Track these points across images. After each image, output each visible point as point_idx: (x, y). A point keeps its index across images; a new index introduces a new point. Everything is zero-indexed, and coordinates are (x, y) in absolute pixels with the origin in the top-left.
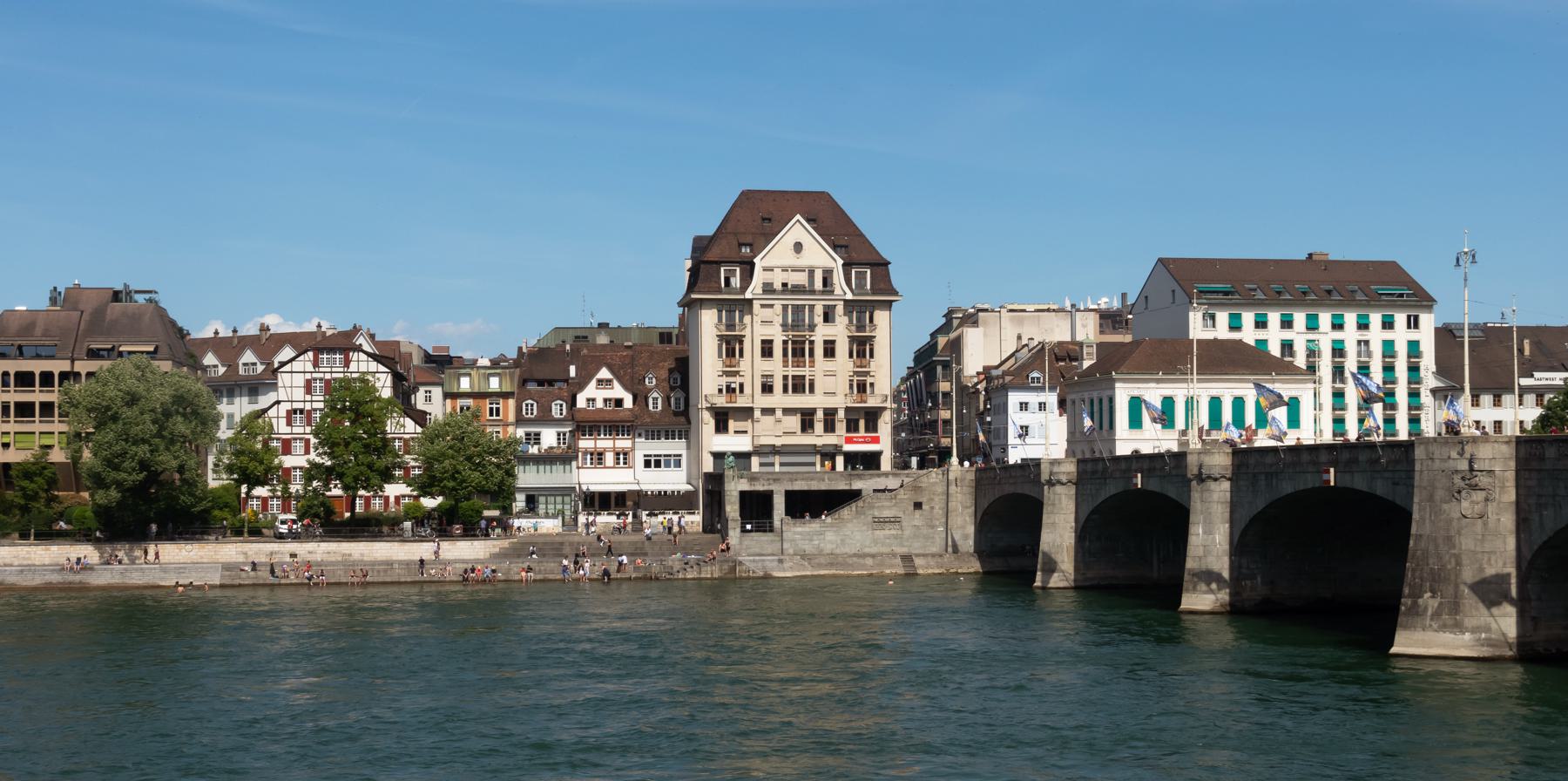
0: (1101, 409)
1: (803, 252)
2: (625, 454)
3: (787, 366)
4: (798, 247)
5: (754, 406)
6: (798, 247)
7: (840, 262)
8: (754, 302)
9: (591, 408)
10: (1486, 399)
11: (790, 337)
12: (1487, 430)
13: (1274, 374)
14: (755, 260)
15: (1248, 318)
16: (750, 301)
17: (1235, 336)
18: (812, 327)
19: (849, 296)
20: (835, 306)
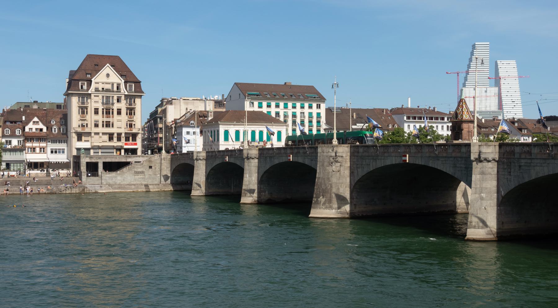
1: (110, 77)
2: (44, 148)
4: (108, 75)
7: (123, 81)
8: (92, 94)
14: (92, 80)
15: (265, 104)
18: (113, 104)
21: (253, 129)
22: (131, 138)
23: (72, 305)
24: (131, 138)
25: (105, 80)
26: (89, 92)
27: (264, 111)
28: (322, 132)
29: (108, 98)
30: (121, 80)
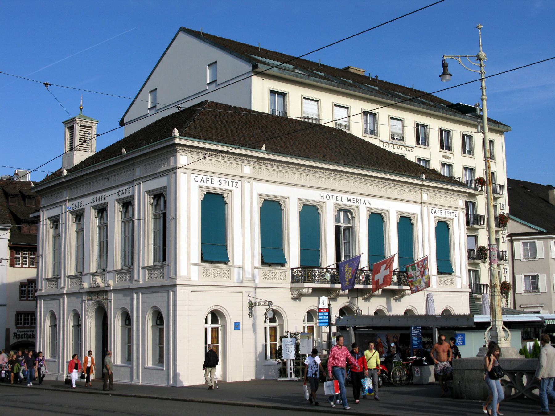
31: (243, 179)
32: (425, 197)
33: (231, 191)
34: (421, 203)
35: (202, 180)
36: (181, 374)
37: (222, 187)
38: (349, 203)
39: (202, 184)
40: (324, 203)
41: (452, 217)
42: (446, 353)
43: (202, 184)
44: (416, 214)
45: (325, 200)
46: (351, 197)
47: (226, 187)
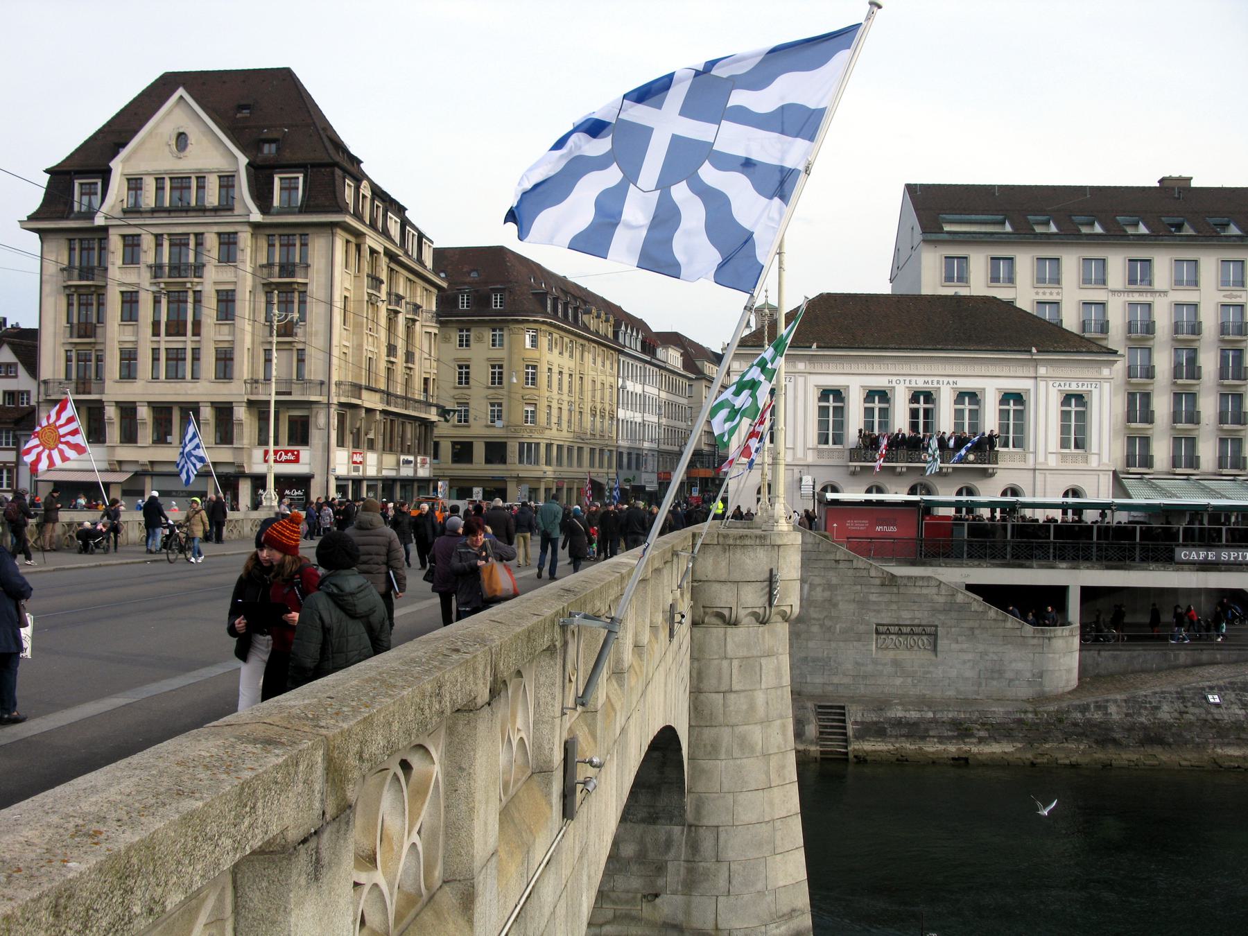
0: (795, 398)
1: (190, 148)
2: (10, 471)
3: (158, 335)
4: (182, 139)
5: (104, 398)
6: (182, 139)
7: (243, 160)
8: (111, 231)
9: (25, 405)
10: (556, 351)
11: (162, 286)
12: (547, 431)
13: (1034, 350)
14: (112, 164)
15: (978, 262)
16: (104, 229)
17: (1002, 294)
18: (199, 269)
19: (256, 216)
20: (236, 233)
21: (920, 383)
22: (922, 398)
23: (556, 842)
24: (922, 398)
25: (170, 163)
26: (99, 221)
27: (1020, 304)
28: (1201, 558)
29: (179, 243)
30: (236, 158)
31: (1102, 381)
32: (1042, 371)
33: (1091, 391)
34: (1036, 378)
35: (1060, 385)
36: (226, 631)
37: (1080, 388)
38: (925, 385)
39: (1060, 388)
40: (894, 387)
41: (1089, 389)
42: (745, 654)
43: (1060, 388)
44: (1029, 390)
45: (894, 384)
46: (926, 379)
47: (1085, 388)
